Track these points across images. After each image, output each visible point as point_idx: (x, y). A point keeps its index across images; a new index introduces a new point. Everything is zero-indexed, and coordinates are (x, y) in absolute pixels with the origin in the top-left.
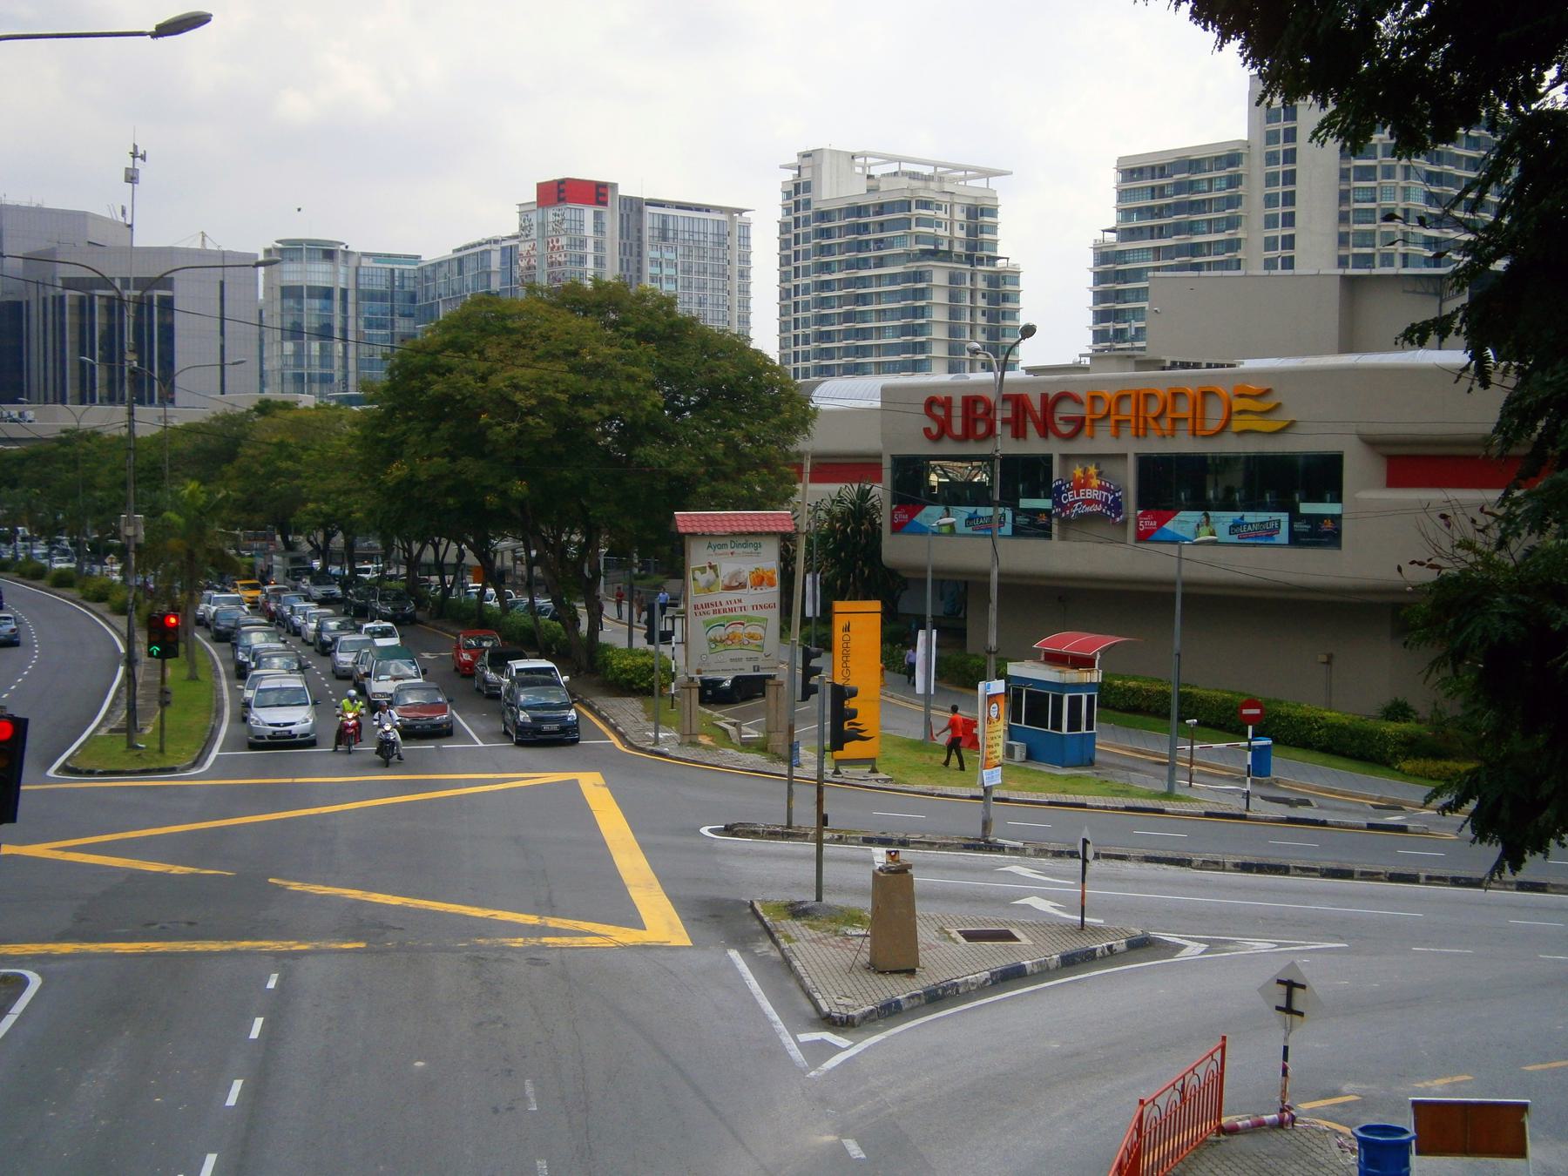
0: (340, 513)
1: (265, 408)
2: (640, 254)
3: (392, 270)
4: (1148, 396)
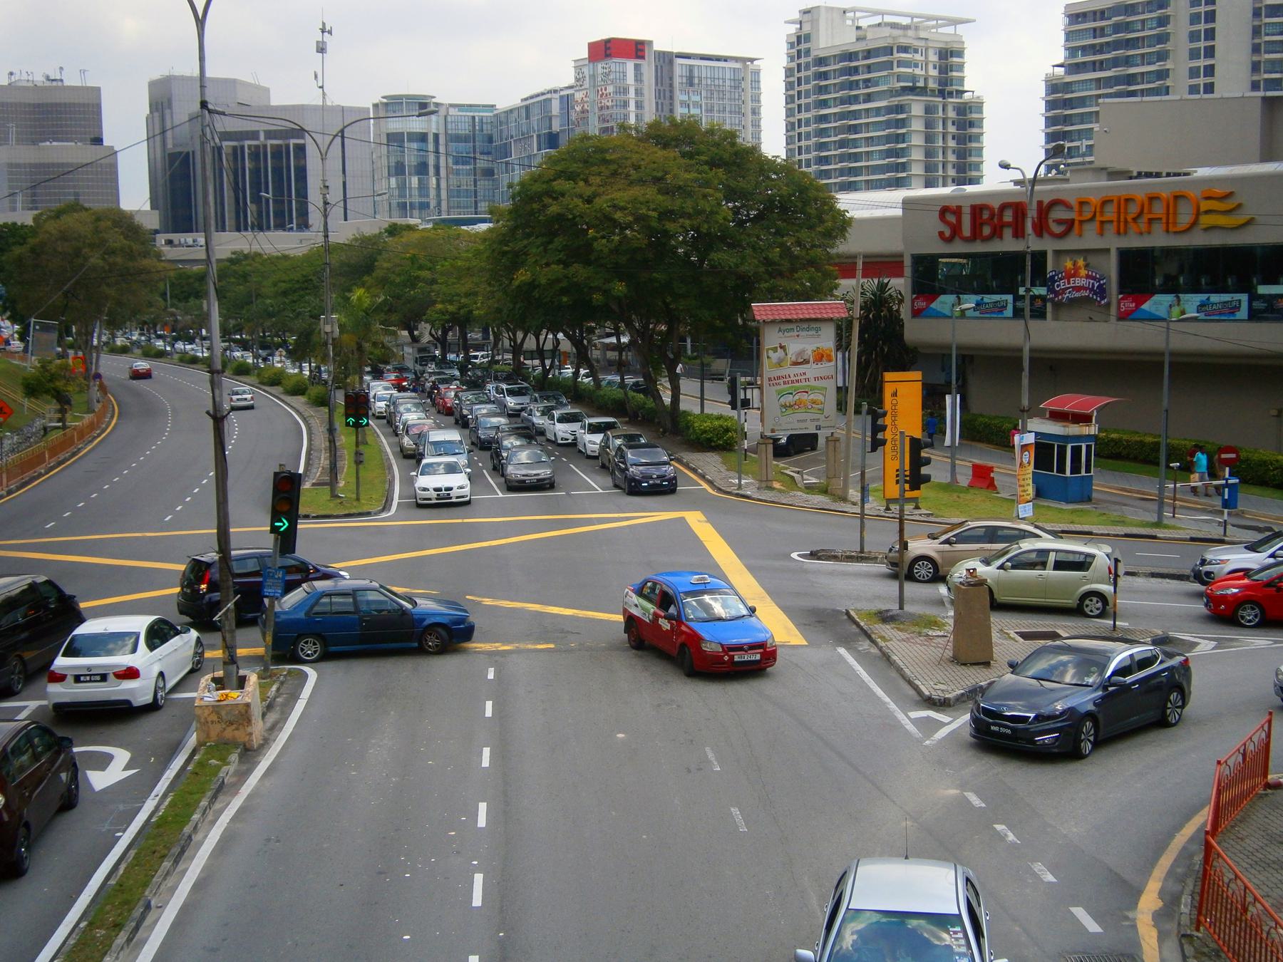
1: (393, 230)
2: (671, 98)
3: (474, 117)
4: (1127, 200)
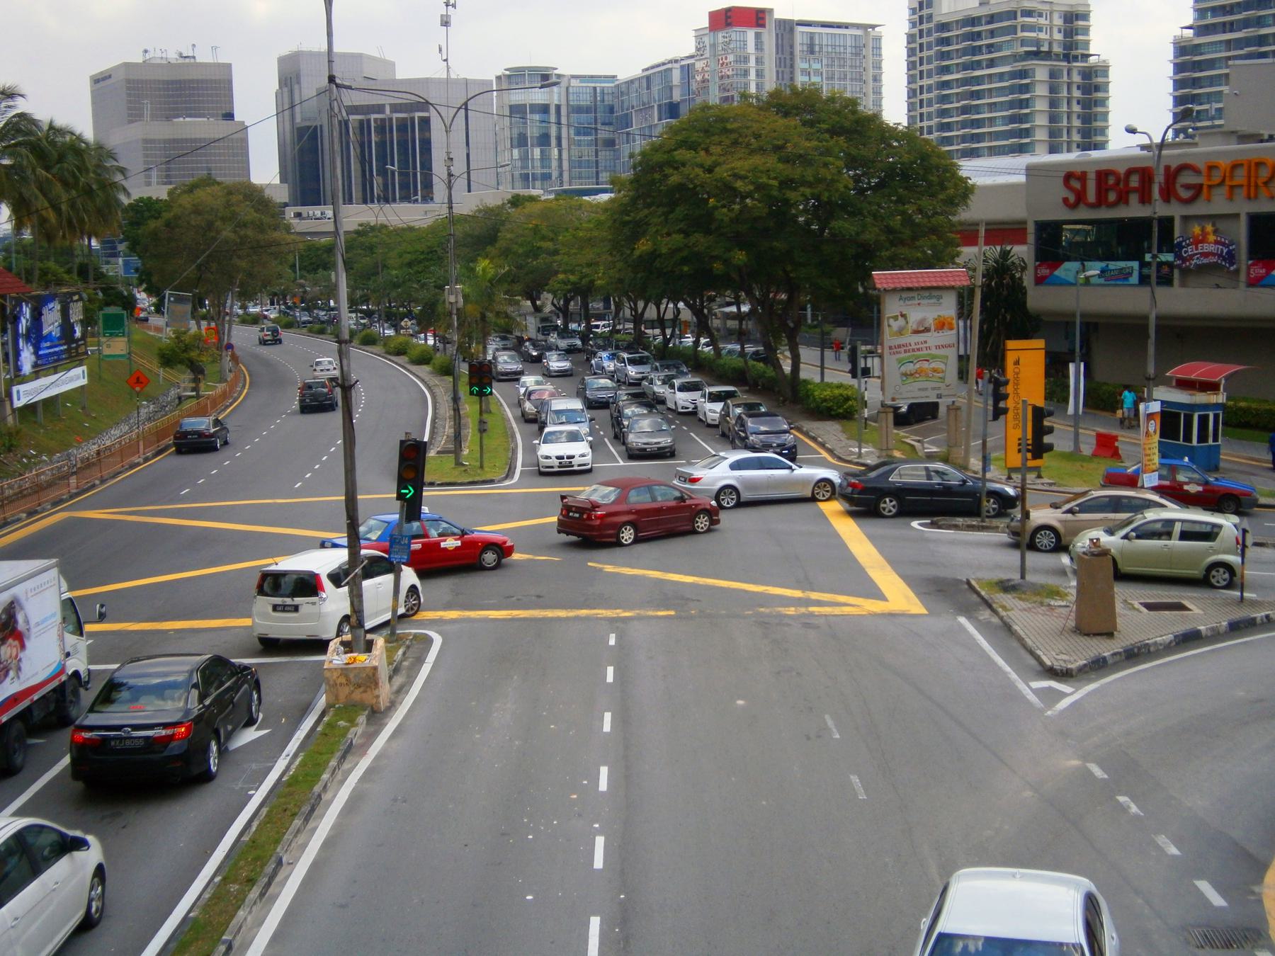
0: (584, 282)
1: (516, 201)
2: (792, 66)
3: (595, 88)
